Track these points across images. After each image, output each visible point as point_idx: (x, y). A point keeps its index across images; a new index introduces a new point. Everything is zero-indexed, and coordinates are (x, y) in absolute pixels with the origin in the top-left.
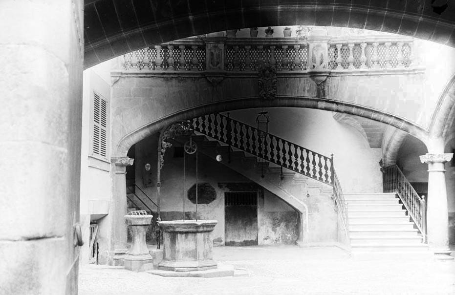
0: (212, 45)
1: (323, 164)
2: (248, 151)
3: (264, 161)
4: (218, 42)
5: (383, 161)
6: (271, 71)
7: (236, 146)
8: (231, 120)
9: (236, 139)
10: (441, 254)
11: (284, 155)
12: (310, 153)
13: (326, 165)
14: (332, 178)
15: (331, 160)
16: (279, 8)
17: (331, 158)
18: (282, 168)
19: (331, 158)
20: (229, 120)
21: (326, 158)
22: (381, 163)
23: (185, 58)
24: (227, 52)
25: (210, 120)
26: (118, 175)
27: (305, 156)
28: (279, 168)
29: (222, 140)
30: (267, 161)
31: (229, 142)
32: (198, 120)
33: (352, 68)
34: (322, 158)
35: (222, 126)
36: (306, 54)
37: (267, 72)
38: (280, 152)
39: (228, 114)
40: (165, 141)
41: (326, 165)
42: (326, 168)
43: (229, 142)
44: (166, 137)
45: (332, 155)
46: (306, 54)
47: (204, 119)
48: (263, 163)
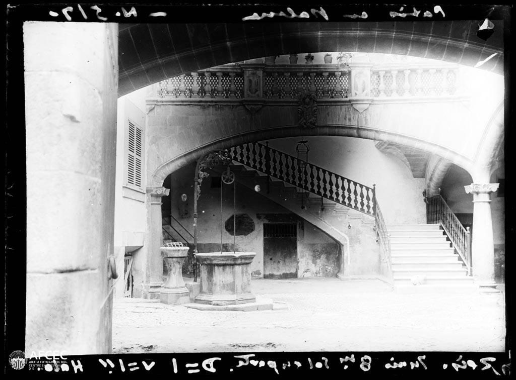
0: (250, 72)
1: (365, 195)
2: (288, 181)
3: (304, 191)
4: (257, 69)
5: (427, 191)
6: (311, 99)
7: (275, 175)
8: (270, 149)
9: (275, 169)
10: (487, 287)
11: (325, 186)
12: (364, 188)
13: (368, 195)
14: (374, 208)
15: (373, 191)
16: (319, 34)
17: (373, 188)
18: (322, 199)
19: (373, 188)
20: (267, 149)
21: (367, 189)
22: (424, 193)
23: (223, 86)
24: (266, 79)
25: (248, 150)
26: (153, 206)
27: (346, 187)
28: (319, 198)
29: (261, 170)
30: (307, 191)
31: (268, 172)
32: (236, 149)
33: (395, 96)
34: (364, 188)
35: (260, 155)
36: (348, 81)
37: (308, 100)
38: (307, 177)
39: (267, 143)
40: (202, 171)
41: (368, 195)
42: (368, 198)
43: (268, 172)
44: (203, 167)
45: (374, 185)
46: (348, 81)
47: (242, 148)
48: (303, 193)
